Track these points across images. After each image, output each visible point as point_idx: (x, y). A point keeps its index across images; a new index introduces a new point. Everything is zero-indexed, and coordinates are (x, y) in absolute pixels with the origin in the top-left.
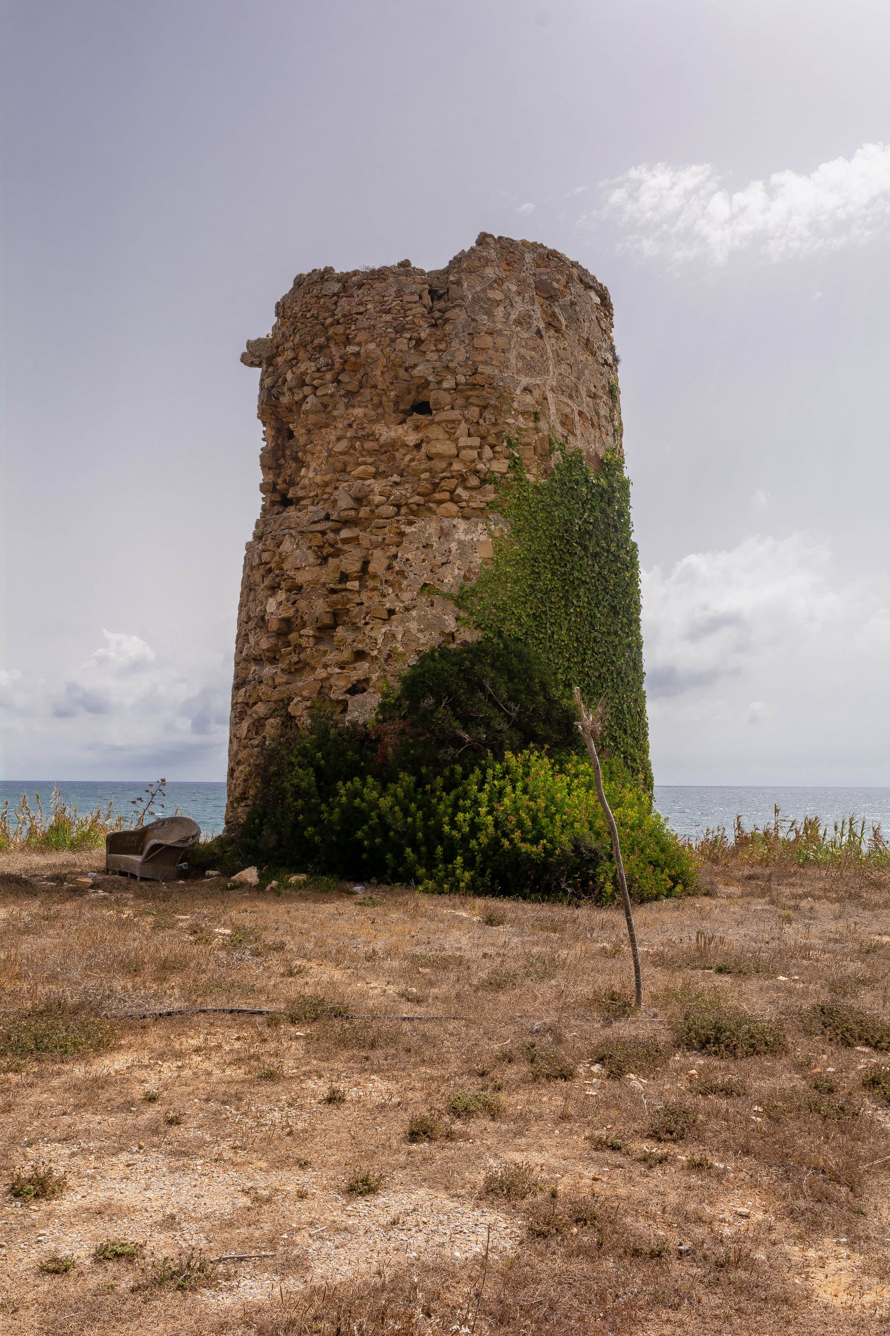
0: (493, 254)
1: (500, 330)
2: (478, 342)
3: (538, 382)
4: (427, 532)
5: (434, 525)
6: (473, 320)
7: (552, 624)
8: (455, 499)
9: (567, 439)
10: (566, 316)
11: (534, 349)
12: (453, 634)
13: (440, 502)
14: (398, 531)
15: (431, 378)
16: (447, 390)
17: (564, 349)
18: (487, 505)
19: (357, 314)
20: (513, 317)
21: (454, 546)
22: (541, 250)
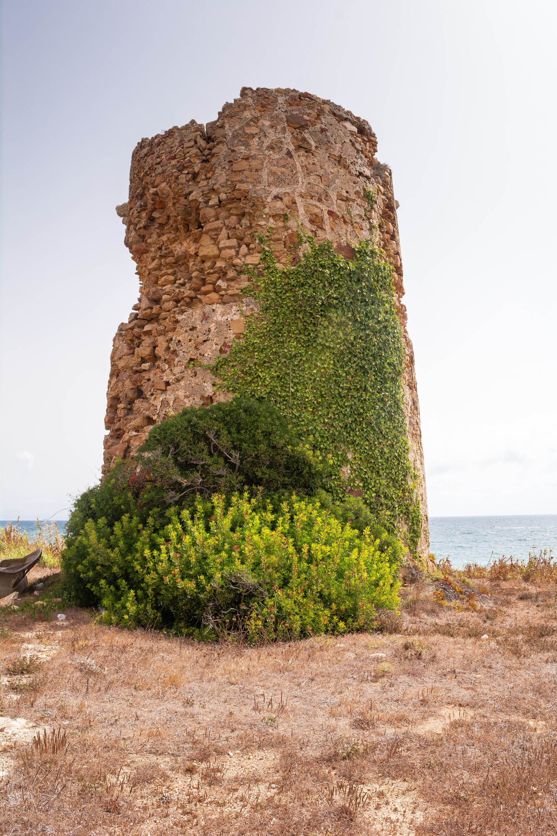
0: (250, 101)
1: (255, 155)
2: (236, 167)
3: (288, 191)
4: (194, 317)
5: (198, 311)
6: (233, 151)
7: (295, 384)
8: (216, 290)
9: (316, 233)
10: (316, 140)
11: (284, 166)
12: (211, 397)
13: (206, 293)
14: (175, 319)
15: (200, 200)
16: (212, 207)
17: (314, 164)
18: (242, 291)
19: (156, 164)
20: (266, 144)
21: (213, 326)
22: (292, 94)
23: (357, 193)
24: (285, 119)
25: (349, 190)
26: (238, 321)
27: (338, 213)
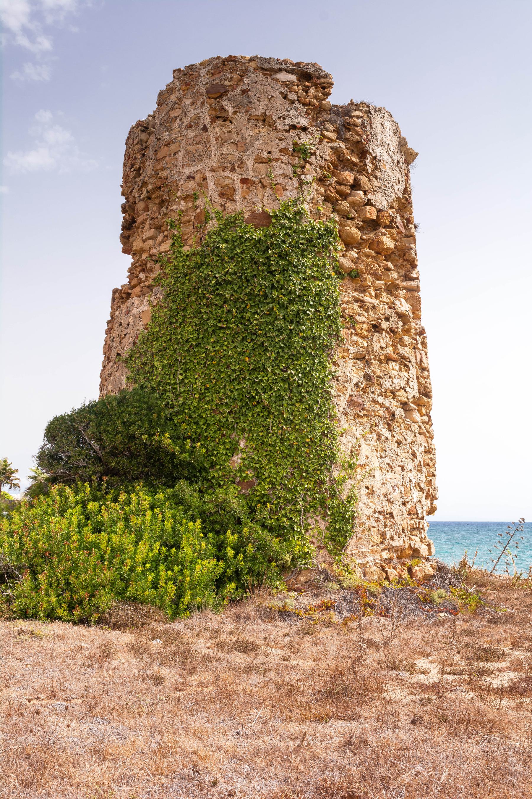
1: (175, 138)
3: (200, 168)
9: (225, 207)
11: (199, 143)
17: (230, 132)
22: (215, 62)
23: (284, 151)
24: (205, 92)
25: (270, 149)
26: (147, 311)
27: (254, 179)
